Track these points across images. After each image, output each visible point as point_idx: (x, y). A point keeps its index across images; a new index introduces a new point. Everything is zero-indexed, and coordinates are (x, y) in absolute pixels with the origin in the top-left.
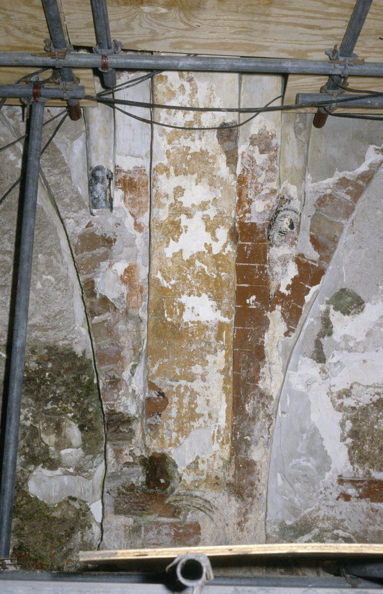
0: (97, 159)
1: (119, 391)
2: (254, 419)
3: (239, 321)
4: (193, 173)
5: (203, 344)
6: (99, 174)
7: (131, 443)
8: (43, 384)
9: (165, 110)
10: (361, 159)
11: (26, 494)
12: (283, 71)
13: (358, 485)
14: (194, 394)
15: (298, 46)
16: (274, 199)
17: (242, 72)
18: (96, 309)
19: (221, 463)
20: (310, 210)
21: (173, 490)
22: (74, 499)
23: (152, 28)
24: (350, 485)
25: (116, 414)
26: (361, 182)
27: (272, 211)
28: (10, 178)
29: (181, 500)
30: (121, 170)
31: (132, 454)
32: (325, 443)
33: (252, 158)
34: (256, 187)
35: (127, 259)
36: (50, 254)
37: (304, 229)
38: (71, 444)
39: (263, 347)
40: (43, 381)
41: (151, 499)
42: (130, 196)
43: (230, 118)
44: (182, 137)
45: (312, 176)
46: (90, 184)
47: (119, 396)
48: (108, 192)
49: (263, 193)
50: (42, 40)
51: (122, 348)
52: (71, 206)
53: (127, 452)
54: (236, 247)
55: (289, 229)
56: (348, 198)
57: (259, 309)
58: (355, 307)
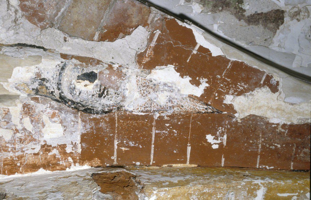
16: (40, 107)
20: (52, 38)
27: (60, 110)
34: (21, 141)
37: (91, 50)
39: (291, 126)
55: (97, 82)
57: (228, 129)
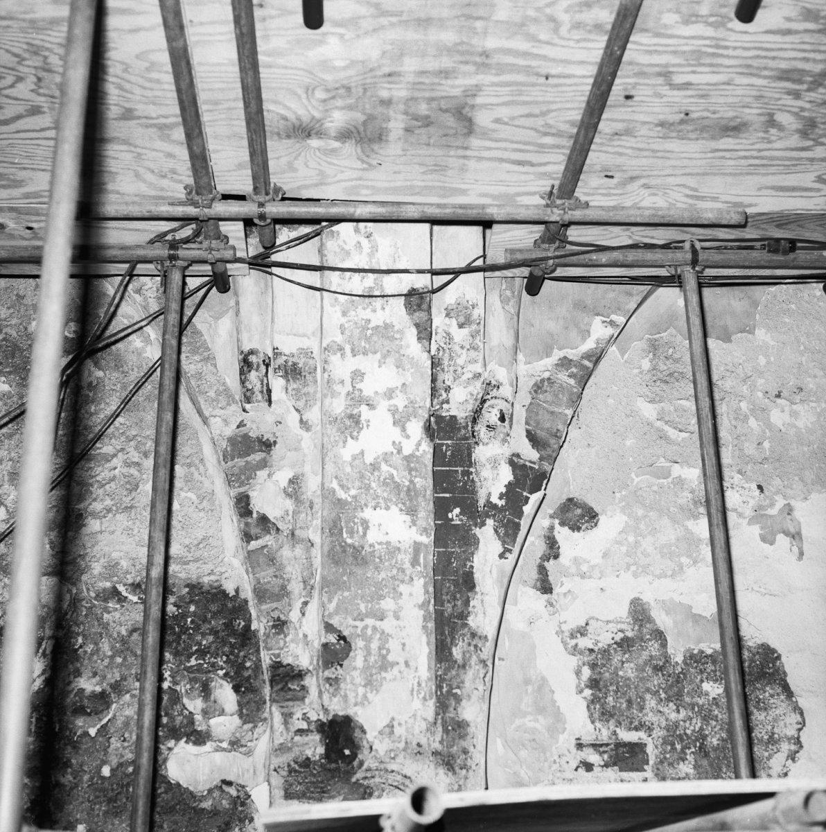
0: (250, 340)
1: (285, 637)
2: (464, 666)
3: (438, 541)
4: (375, 353)
5: (395, 571)
6: (253, 359)
7: (304, 704)
8: (184, 633)
9: (338, 273)
10: (586, 334)
11: (165, 780)
12: (487, 218)
13: (601, 749)
14: (385, 637)
15: (504, 188)
17: (435, 222)
18: (254, 531)
19: (424, 726)
20: (524, 398)
21: (361, 764)
22: (229, 784)
23: (322, 168)
24: (591, 750)
25: (283, 666)
26: (586, 363)
27: (476, 400)
28: (136, 369)
29: (373, 777)
30: (281, 354)
31: (305, 718)
32: (556, 697)
33: (449, 334)
35: (293, 466)
36: (189, 465)
38: (223, 710)
39: (472, 573)
40: (184, 630)
41: (333, 777)
42: (293, 385)
43: (422, 282)
44: (360, 307)
45: (525, 356)
46: (242, 373)
47: (285, 642)
48: (265, 381)
49: (465, 377)
50: (181, 187)
51: (289, 580)
52: (218, 401)
53: (299, 715)
54: (432, 445)
55: (499, 423)
56: (572, 381)
58: (587, 522)
